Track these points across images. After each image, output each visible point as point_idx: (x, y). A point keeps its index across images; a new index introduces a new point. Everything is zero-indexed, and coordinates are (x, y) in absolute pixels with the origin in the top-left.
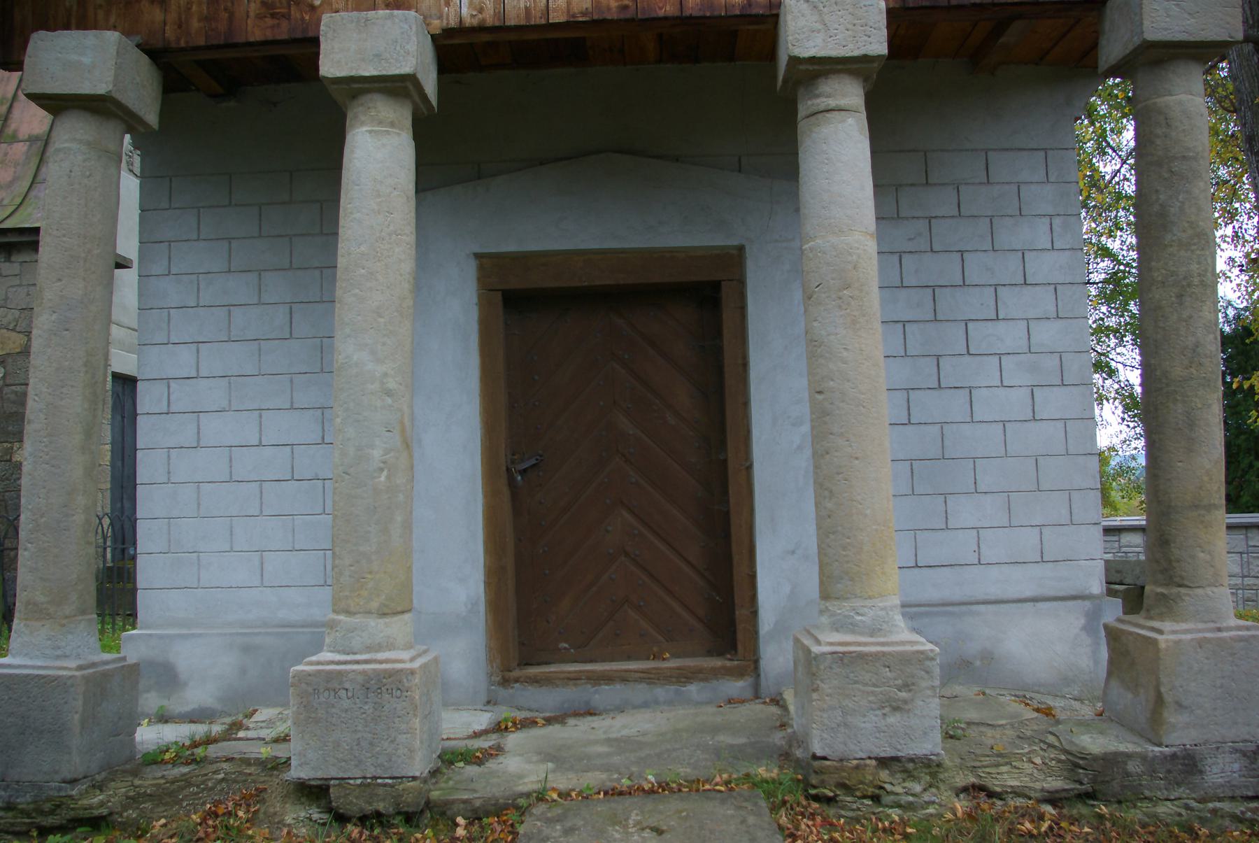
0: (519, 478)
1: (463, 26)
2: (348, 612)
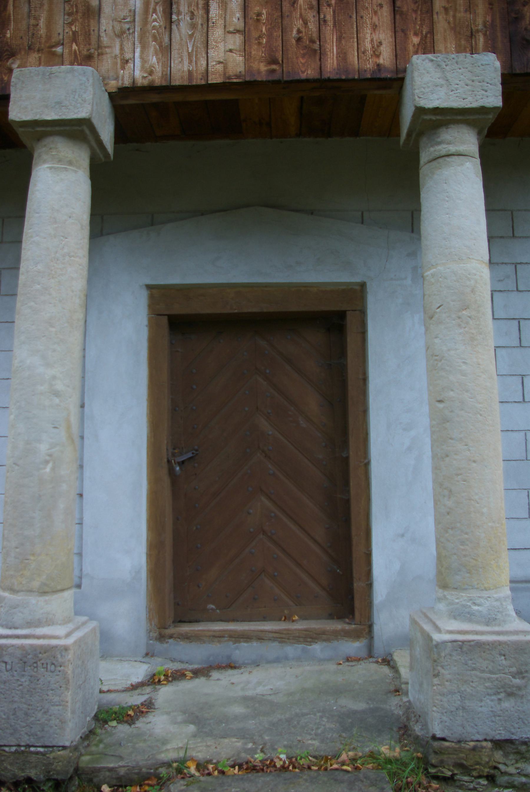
0: (178, 468)
1: (136, 85)
2: (12, 590)
